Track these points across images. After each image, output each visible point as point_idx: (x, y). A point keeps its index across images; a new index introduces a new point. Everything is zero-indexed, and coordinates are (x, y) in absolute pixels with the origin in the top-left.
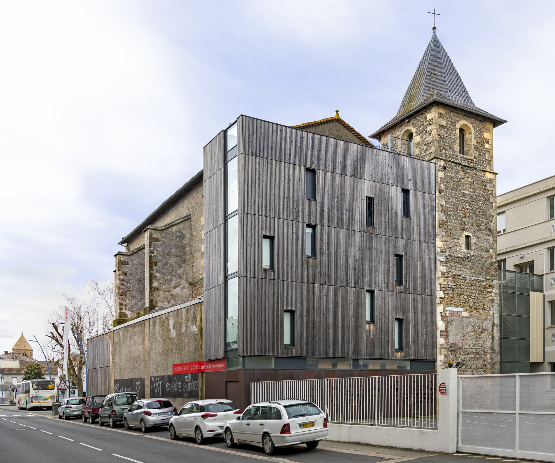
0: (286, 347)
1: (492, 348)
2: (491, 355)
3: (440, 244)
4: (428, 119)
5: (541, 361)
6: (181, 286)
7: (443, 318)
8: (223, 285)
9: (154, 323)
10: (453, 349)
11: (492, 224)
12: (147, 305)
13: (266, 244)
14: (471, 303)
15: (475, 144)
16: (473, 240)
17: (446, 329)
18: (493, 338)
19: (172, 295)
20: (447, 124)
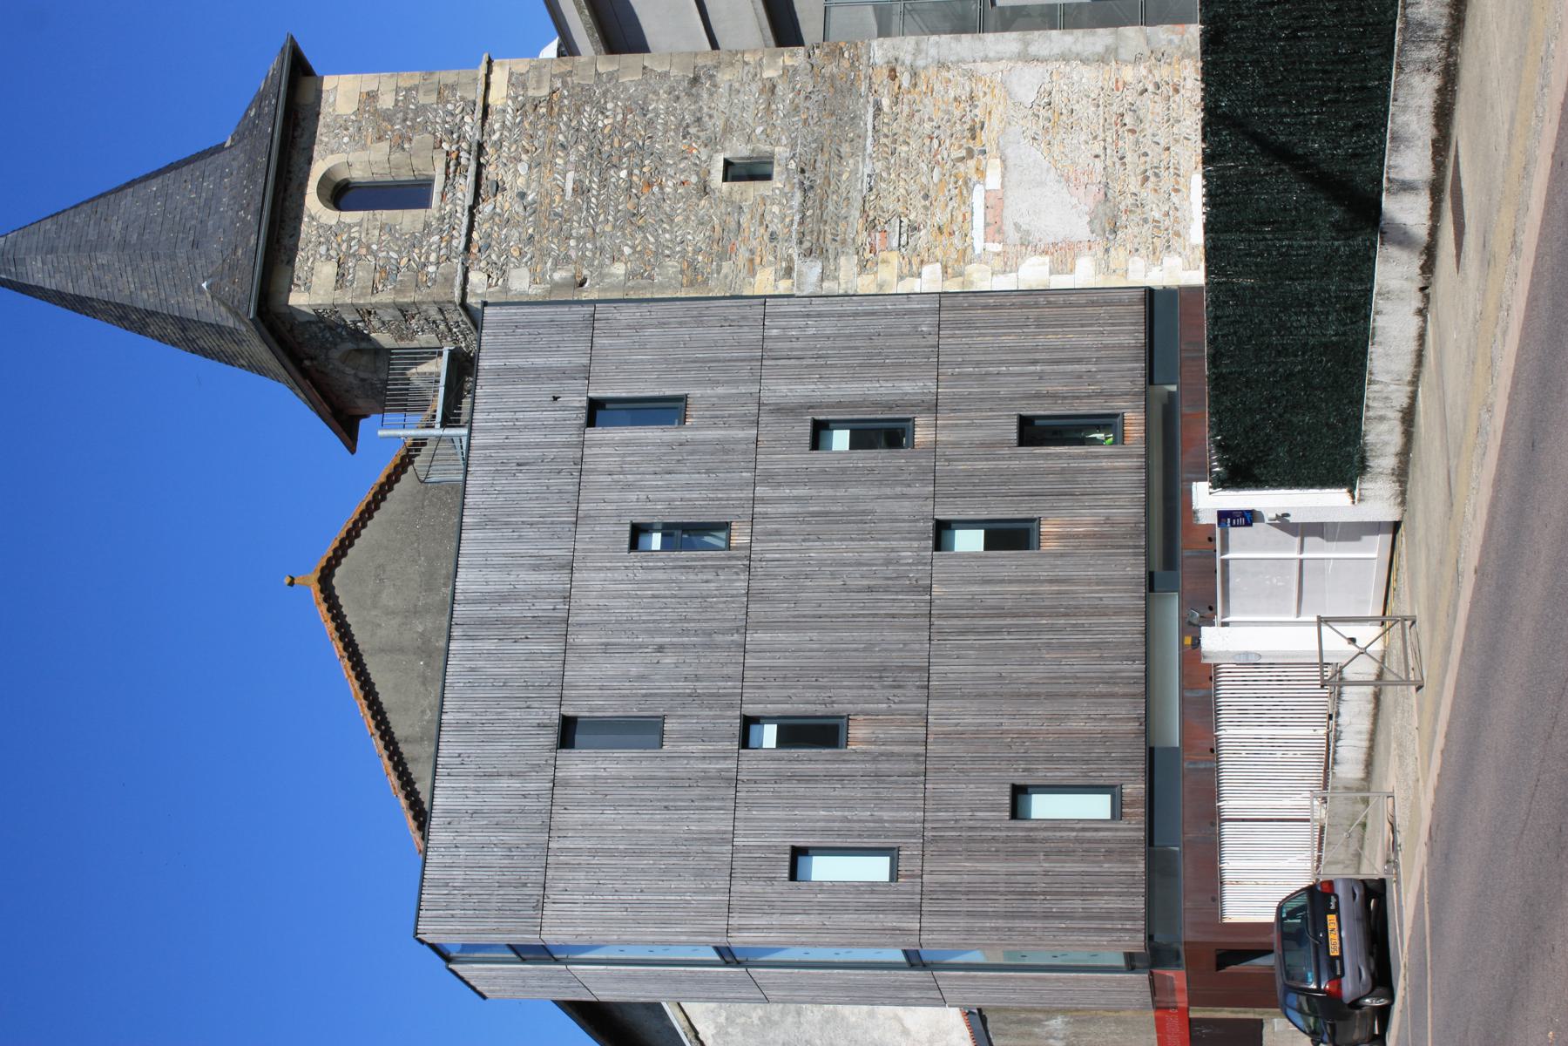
0: (1117, 811)
1: (1102, 59)
2: (1126, 62)
3: (765, 282)
13: (823, 869)
15: (385, 146)
16: (739, 149)
17: (1045, 252)
18: (1065, 58)
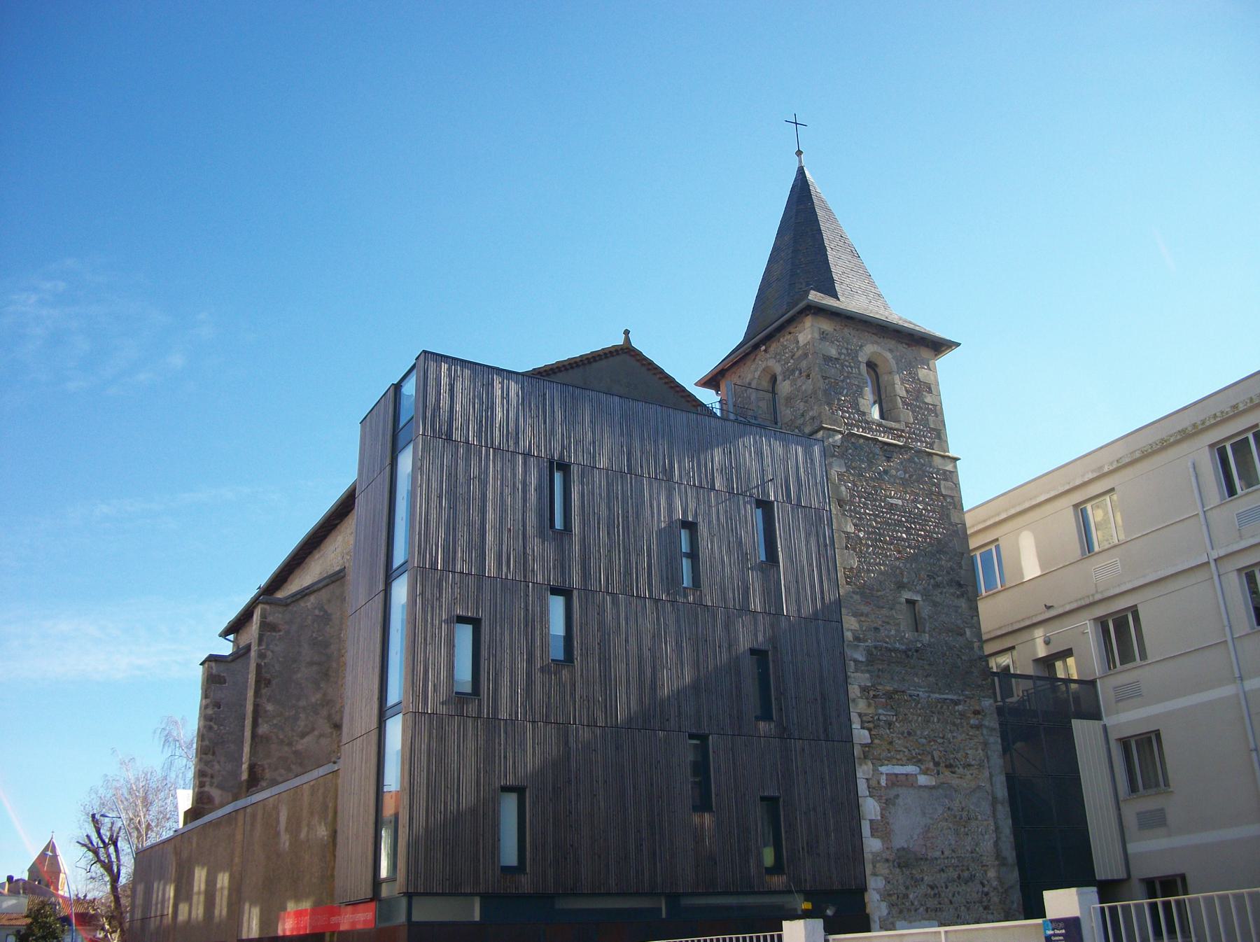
1: (998, 855)
4: (801, 344)
5: (1124, 876)
6: (316, 733)
7: (873, 790)
8: (376, 731)
9: (254, 816)
10: (904, 861)
11: (963, 572)
12: (245, 776)
13: (464, 634)
14: (936, 754)
15: (904, 394)
19: (296, 753)
20: (840, 354)
